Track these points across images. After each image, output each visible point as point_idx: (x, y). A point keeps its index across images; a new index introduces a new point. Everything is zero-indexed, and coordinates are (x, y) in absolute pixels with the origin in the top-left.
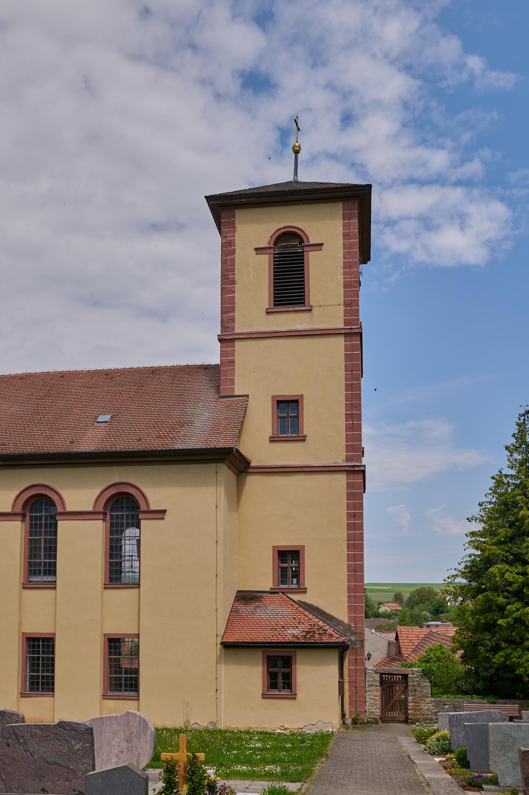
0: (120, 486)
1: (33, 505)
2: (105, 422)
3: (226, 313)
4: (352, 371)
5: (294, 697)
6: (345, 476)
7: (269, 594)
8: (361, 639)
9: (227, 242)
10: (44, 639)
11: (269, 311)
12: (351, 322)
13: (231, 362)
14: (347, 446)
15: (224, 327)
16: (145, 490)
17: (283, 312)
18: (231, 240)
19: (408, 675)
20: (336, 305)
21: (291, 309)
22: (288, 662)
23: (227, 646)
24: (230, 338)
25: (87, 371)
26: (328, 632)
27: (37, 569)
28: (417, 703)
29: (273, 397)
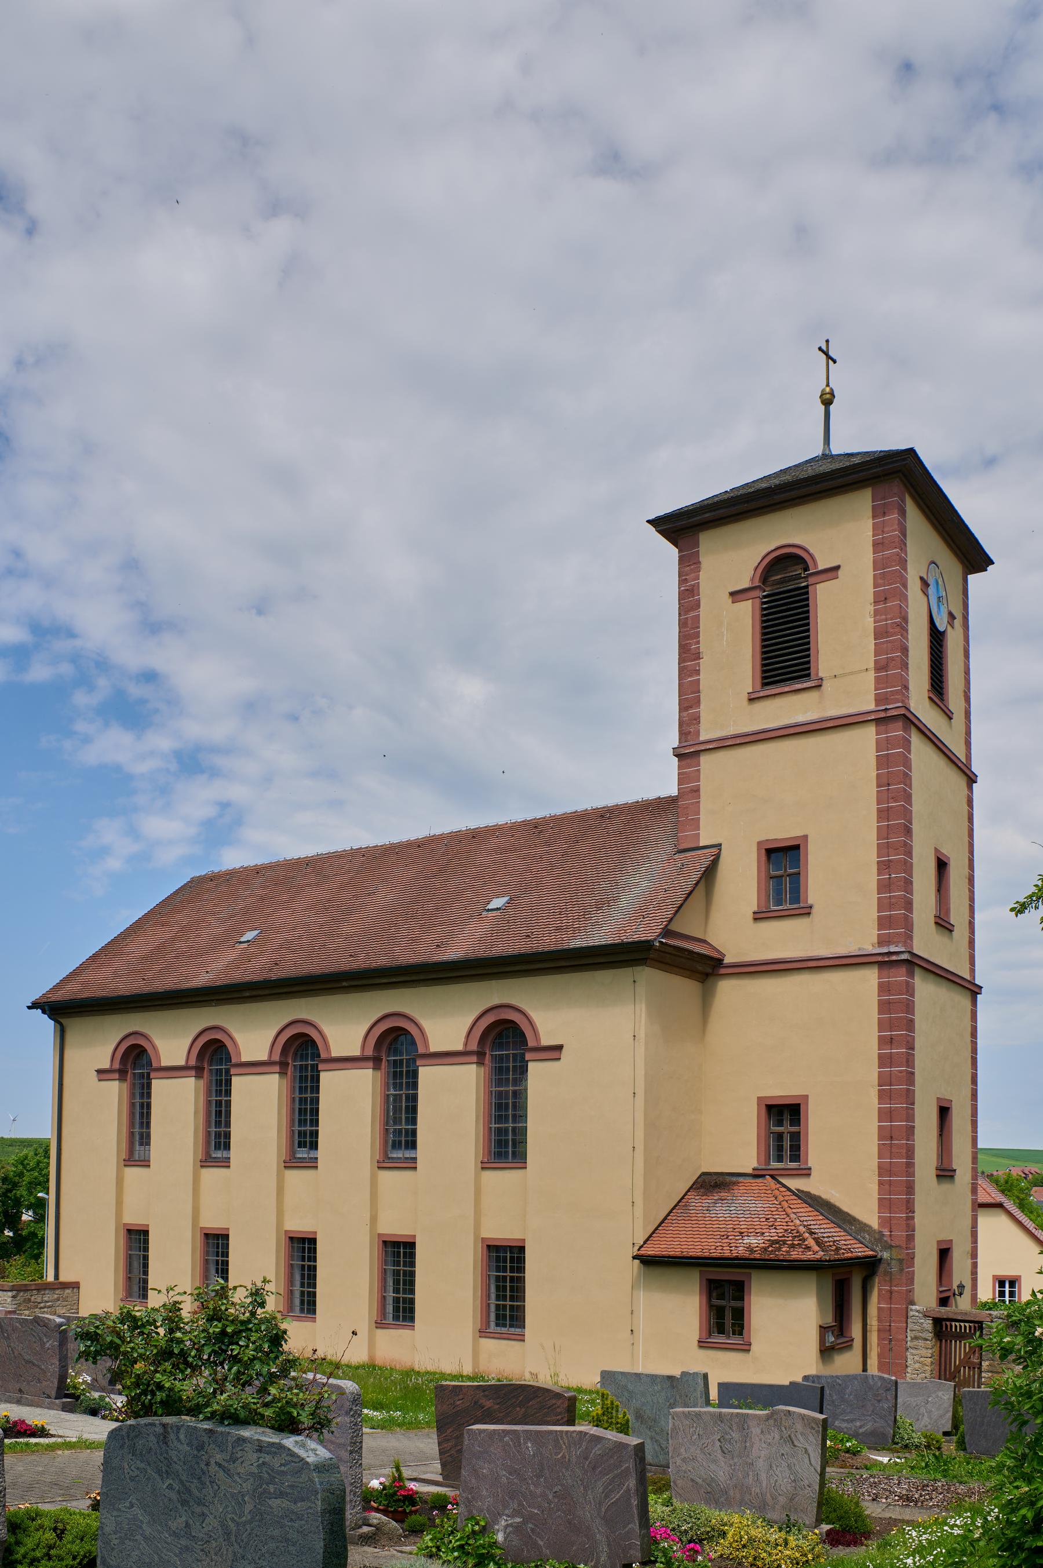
0: (501, 1010)
1: (391, 1044)
2: (498, 909)
3: (687, 708)
4: (889, 785)
5: (746, 1348)
6: (876, 971)
7: (751, 1178)
8: (899, 1257)
9: (687, 590)
11: (753, 697)
14: (880, 918)
15: (683, 734)
17: (775, 695)
18: (693, 586)
20: (861, 671)
21: (787, 689)
22: (739, 1290)
23: (648, 1262)
24: (691, 750)
25: (513, 823)
26: (806, 1243)
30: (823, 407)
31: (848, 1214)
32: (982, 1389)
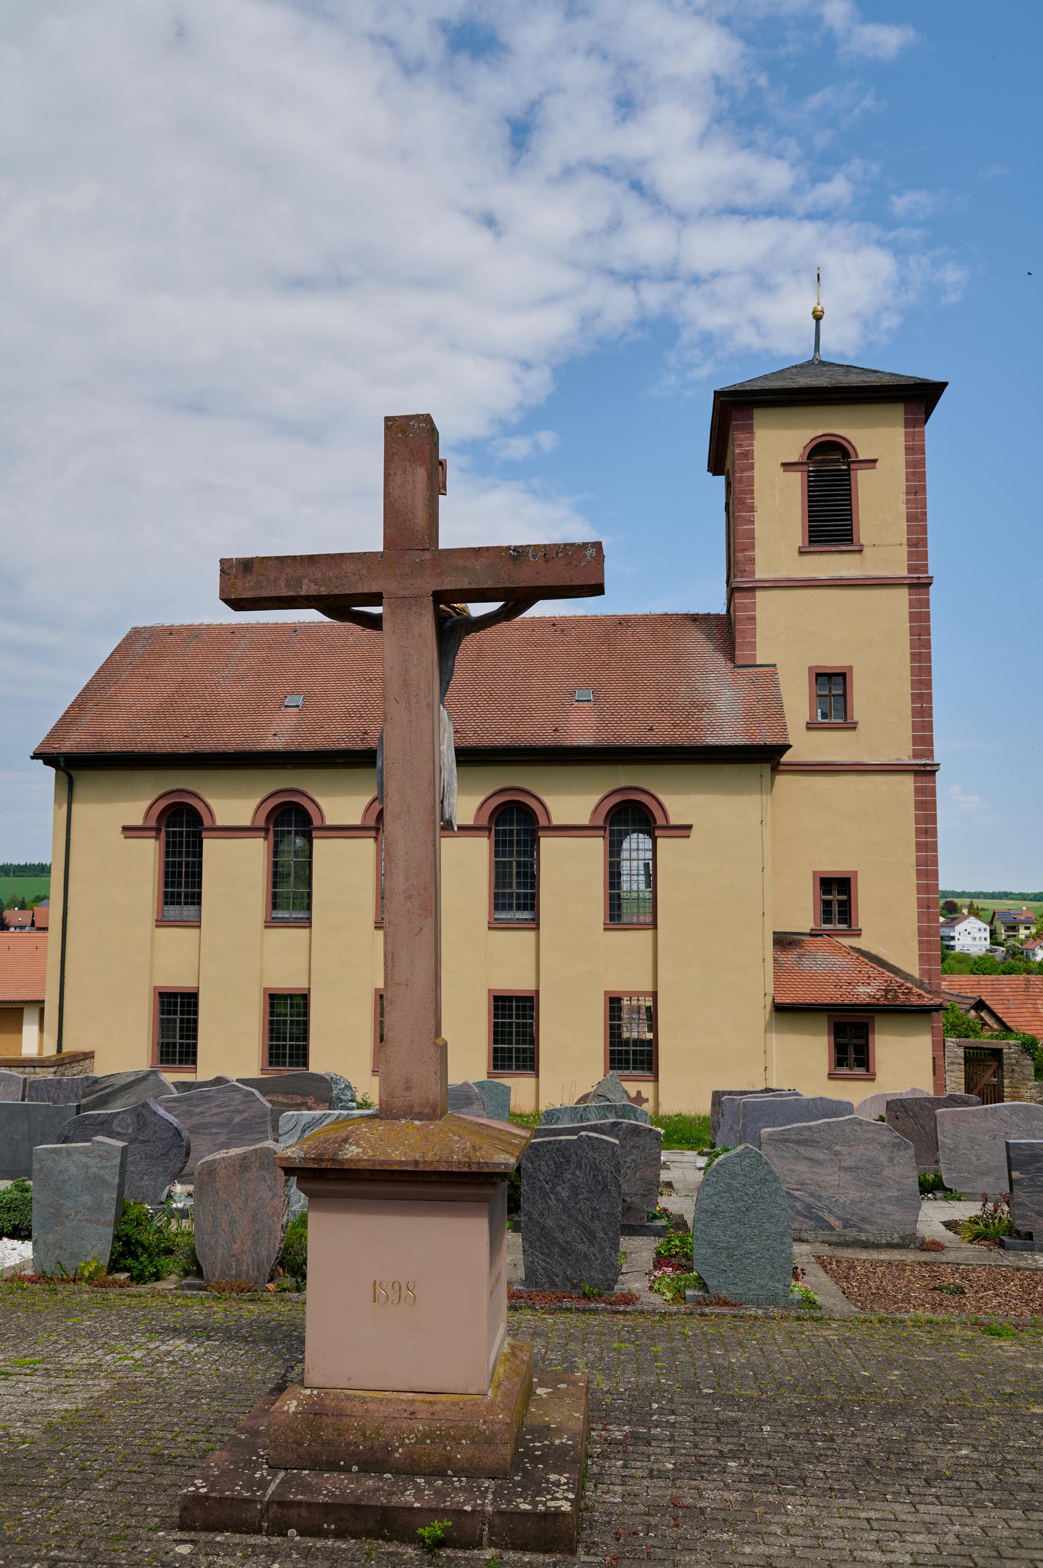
1: (499, 815)
4: (920, 635)
6: (913, 777)
10: (183, 995)
12: (917, 569)
13: (752, 619)
16: (662, 798)
17: (822, 552)
18: (748, 451)
19: (1002, 1049)
20: (896, 545)
21: (834, 549)
23: (780, 1009)
27: (507, 902)
28: (1016, 1088)
29: (810, 668)
30: (814, 321)
31: (894, 967)
32: (26, 1102)
